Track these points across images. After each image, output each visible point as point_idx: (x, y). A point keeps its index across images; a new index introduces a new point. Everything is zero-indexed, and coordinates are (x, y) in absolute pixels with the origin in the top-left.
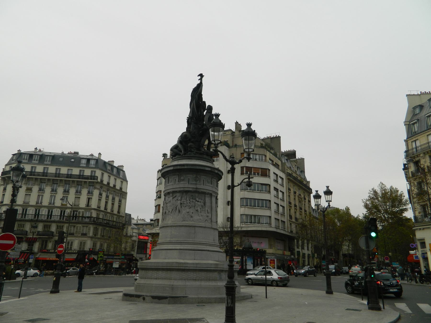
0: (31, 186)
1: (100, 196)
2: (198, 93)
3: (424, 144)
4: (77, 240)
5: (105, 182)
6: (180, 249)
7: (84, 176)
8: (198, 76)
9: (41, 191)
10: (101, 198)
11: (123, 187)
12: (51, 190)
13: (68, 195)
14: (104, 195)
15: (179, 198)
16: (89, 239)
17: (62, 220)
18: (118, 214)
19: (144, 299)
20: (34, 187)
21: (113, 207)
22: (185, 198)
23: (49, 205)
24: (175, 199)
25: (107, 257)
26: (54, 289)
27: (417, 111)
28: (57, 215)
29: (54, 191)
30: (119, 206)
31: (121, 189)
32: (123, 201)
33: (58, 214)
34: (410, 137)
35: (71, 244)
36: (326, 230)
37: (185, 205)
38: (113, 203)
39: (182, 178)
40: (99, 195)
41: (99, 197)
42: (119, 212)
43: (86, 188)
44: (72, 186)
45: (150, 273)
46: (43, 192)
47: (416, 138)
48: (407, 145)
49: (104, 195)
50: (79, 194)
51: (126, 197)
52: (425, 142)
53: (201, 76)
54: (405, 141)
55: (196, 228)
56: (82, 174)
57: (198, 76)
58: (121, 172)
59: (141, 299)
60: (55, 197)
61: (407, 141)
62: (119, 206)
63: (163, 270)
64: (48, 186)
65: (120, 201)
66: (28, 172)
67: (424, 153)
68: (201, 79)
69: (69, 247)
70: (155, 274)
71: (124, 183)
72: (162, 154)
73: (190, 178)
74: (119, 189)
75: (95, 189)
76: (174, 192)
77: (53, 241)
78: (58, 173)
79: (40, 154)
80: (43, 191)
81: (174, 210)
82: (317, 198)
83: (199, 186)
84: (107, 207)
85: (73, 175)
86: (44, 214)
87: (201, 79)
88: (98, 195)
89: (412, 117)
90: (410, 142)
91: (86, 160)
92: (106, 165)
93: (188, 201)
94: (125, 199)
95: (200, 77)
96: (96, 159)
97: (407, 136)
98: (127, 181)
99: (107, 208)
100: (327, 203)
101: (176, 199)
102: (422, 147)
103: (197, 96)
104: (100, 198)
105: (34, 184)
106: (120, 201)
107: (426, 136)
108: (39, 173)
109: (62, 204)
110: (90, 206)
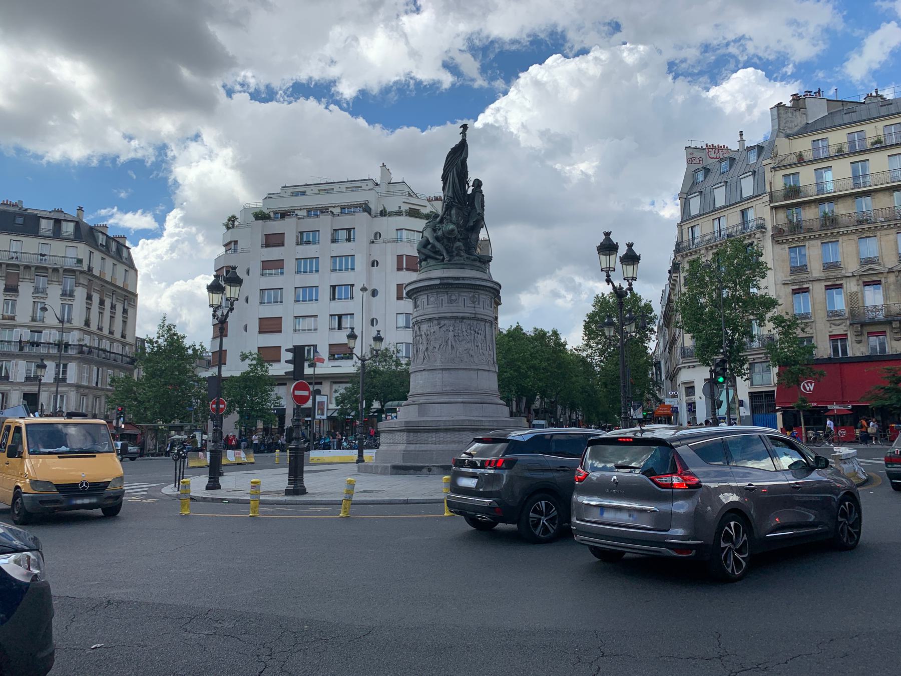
2: (462, 158)
3: (707, 235)
4: (16, 390)
5: (96, 272)
6: (462, 403)
9: (38, 292)
10: (91, 304)
12: (32, 290)
14: (96, 298)
15: (451, 328)
16: (73, 389)
18: (86, 328)
19: (430, 470)
20: (49, 286)
22: (460, 328)
24: (444, 329)
26: (509, 438)
27: (700, 176)
29: (67, 294)
32: (130, 311)
34: (687, 220)
37: (460, 339)
39: (453, 298)
41: (87, 303)
42: (123, 336)
43: (57, 283)
44: (25, 277)
45: (424, 436)
46: (45, 296)
47: (696, 223)
48: (681, 232)
49: (96, 298)
50: (42, 296)
52: (710, 231)
54: (678, 225)
55: (479, 372)
58: (125, 250)
59: (425, 470)
61: (681, 226)
63: (447, 430)
64: (24, 280)
65: (125, 311)
67: (707, 249)
68: (464, 133)
70: (433, 437)
73: (465, 298)
75: (77, 285)
76: (430, 319)
80: (43, 293)
81: (442, 346)
82: (232, 284)
83: (480, 310)
87: (464, 133)
89: (691, 188)
90: (685, 227)
92: (96, 234)
93: (465, 333)
94: (135, 306)
97: (682, 218)
98: (136, 270)
100: (604, 274)
101: (445, 330)
102: (704, 239)
103: (459, 162)
104: (88, 306)
105: (50, 282)
106: (125, 311)
107: (711, 221)
109: (3, 317)
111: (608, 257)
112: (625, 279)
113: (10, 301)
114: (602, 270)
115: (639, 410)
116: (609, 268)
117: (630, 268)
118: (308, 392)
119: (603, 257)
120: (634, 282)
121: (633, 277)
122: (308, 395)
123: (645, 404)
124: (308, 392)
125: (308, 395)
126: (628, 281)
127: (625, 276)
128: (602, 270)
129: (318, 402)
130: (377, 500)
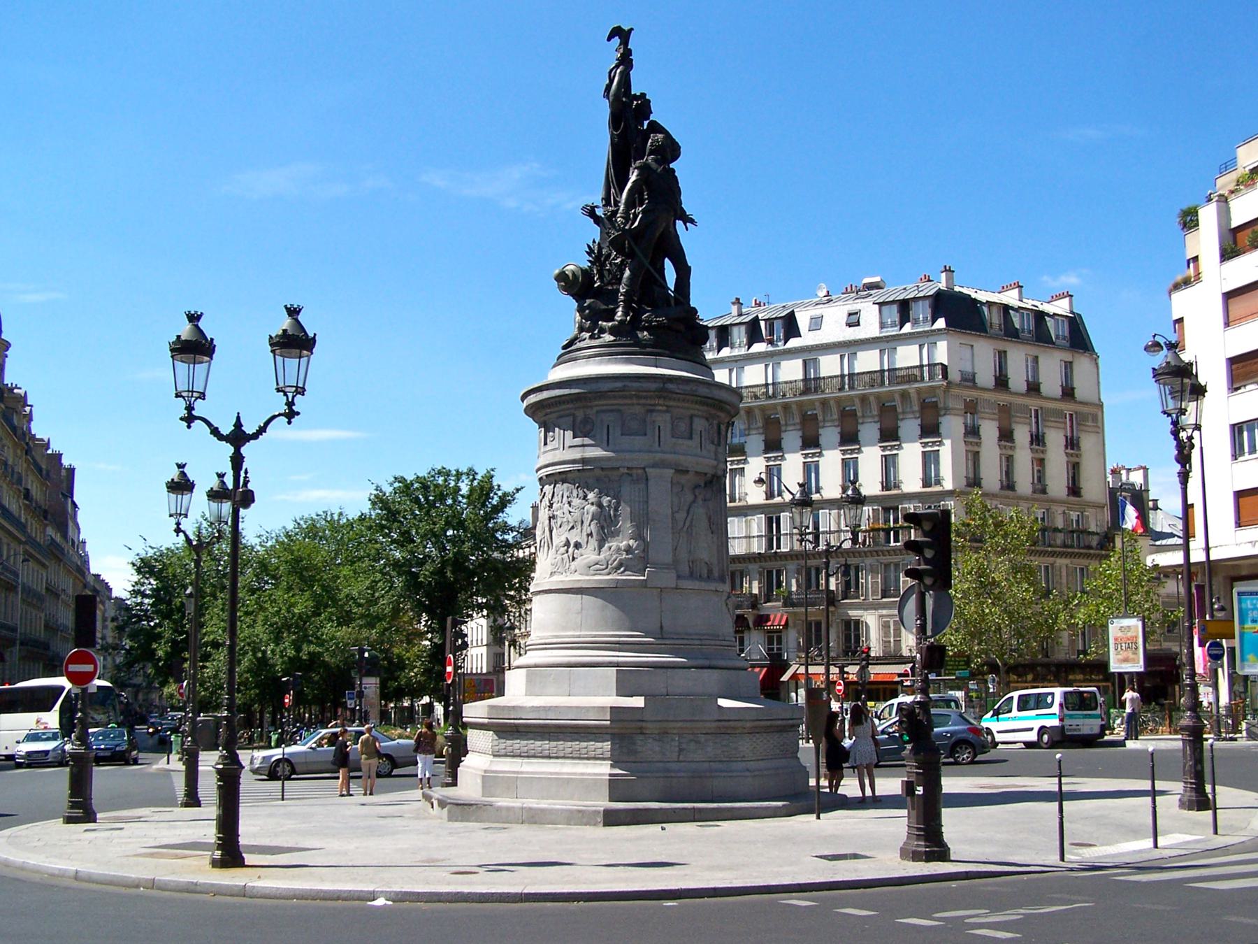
0: (743, 440)
1: (971, 440)
7: (898, 373)
8: (609, 39)
11: (1077, 384)
13: (856, 453)
17: (892, 544)
18: (1072, 498)
21: (1044, 474)
23: (767, 499)
25: (450, 665)
28: (758, 536)
30: (1074, 470)
31: (1068, 393)
32: (1087, 442)
33: (759, 530)
35: (894, 630)
36: (193, 577)
38: (1075, 459)
40: (965, 437)
42: (1074, 490)
51: (1100, 424)
53: (621, 34)
55: (1210, 546)
56: (812, 377)
57: (609, 39)
60: (780, 469)
62: (1074, 470)
65: (1072, 444)
66: (875, 372)
69: (892, 640)
71: (1082, 364)
72: (1177, 211)
74: (1058, 392)
77: (838, 623)
78: (929, 365)
79: (747, 320)
84: (1013, 478)
85: (858, 374)
86: (756, 534)
88: (962, 435)
91: (895, 308)
95: (616, 40)
96: (929, 296)
99: (1015, 480)
100: (182, 403)
104: (970, 448)
106: (1072, 444)
108: (754, 390)
110: (897, 486)
111: (192, 366)
112: (278, 390)
113: (851, 461)
114: (177, 396)
115: (839, 705)
116: (193, 392)
117: (292, 363)
118: (92, 666)
119: (182, 367)
120: (298, 398)
121: (297, 387)
122: (70, 666)
123: (1241, 705)
124: (92, 666)
125: (70, 666)
126: (285, 394)
127: (281, 385)
128: (177, 396)
129: (529, 693)
130: (334, 891)
